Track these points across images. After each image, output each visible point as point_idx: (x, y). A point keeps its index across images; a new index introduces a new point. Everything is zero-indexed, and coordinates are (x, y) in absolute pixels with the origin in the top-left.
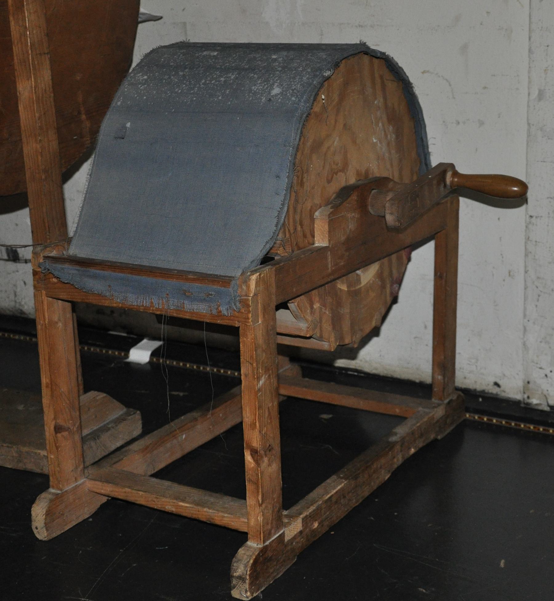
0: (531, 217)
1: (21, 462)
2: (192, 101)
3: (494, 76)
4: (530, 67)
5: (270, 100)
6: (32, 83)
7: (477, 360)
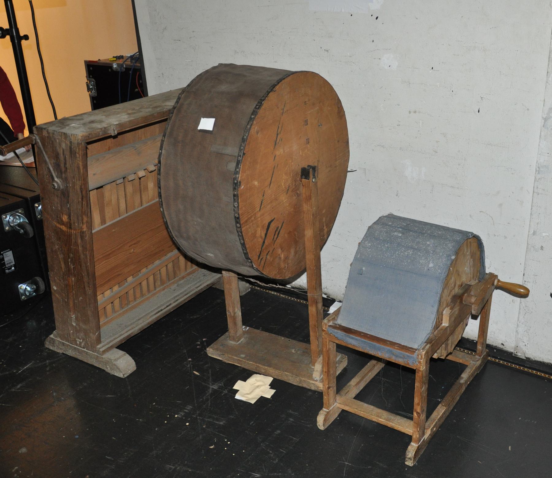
0: (525, 281)
2: (393, 262)
3: (513, 219)
4: (530, 221)
5: (429, 270)
7: (495, 333)
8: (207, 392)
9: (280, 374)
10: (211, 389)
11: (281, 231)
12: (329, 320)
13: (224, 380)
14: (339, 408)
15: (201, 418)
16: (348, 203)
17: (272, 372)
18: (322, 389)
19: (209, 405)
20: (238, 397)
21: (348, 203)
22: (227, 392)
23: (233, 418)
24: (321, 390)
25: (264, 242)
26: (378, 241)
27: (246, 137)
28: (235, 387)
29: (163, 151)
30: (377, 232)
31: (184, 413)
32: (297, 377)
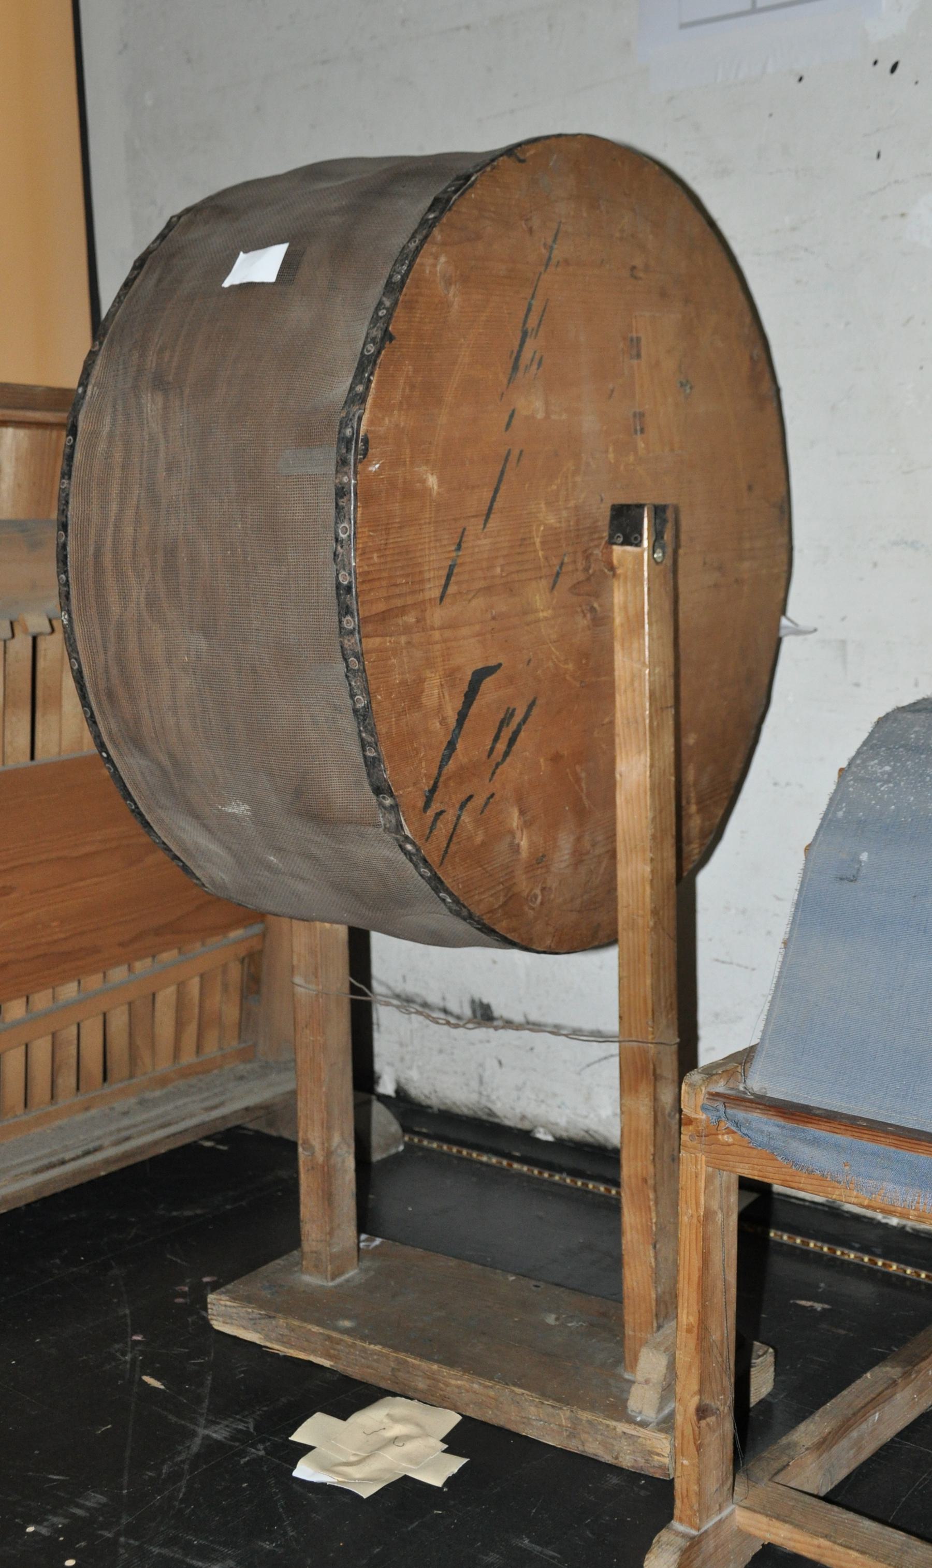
1: (575, 1437)
6: (646, 761)
8: (180, 1448)
9: (492, 1393)
10: (198, 1441)
11: (522, 734)
12: (712, 1075)
13: (258, 1413)
14: (744, 1535)
15: (132, 1542)
16: (775, 784)
17: (459, 1387)
18: (666, 1461)
19: (181, 1495)
20: (304, 1471)
21: (775, 784)
22: (262, 1453)
23: (270, 1551)
24: (663, 1468)
25: (451, 746)
26: (923, 756)
27: (399, 277)
28: (300, 1436)
29: (90, 388)
30: (916, 729)
31: (66, 1521)
32: (561, 1409)
